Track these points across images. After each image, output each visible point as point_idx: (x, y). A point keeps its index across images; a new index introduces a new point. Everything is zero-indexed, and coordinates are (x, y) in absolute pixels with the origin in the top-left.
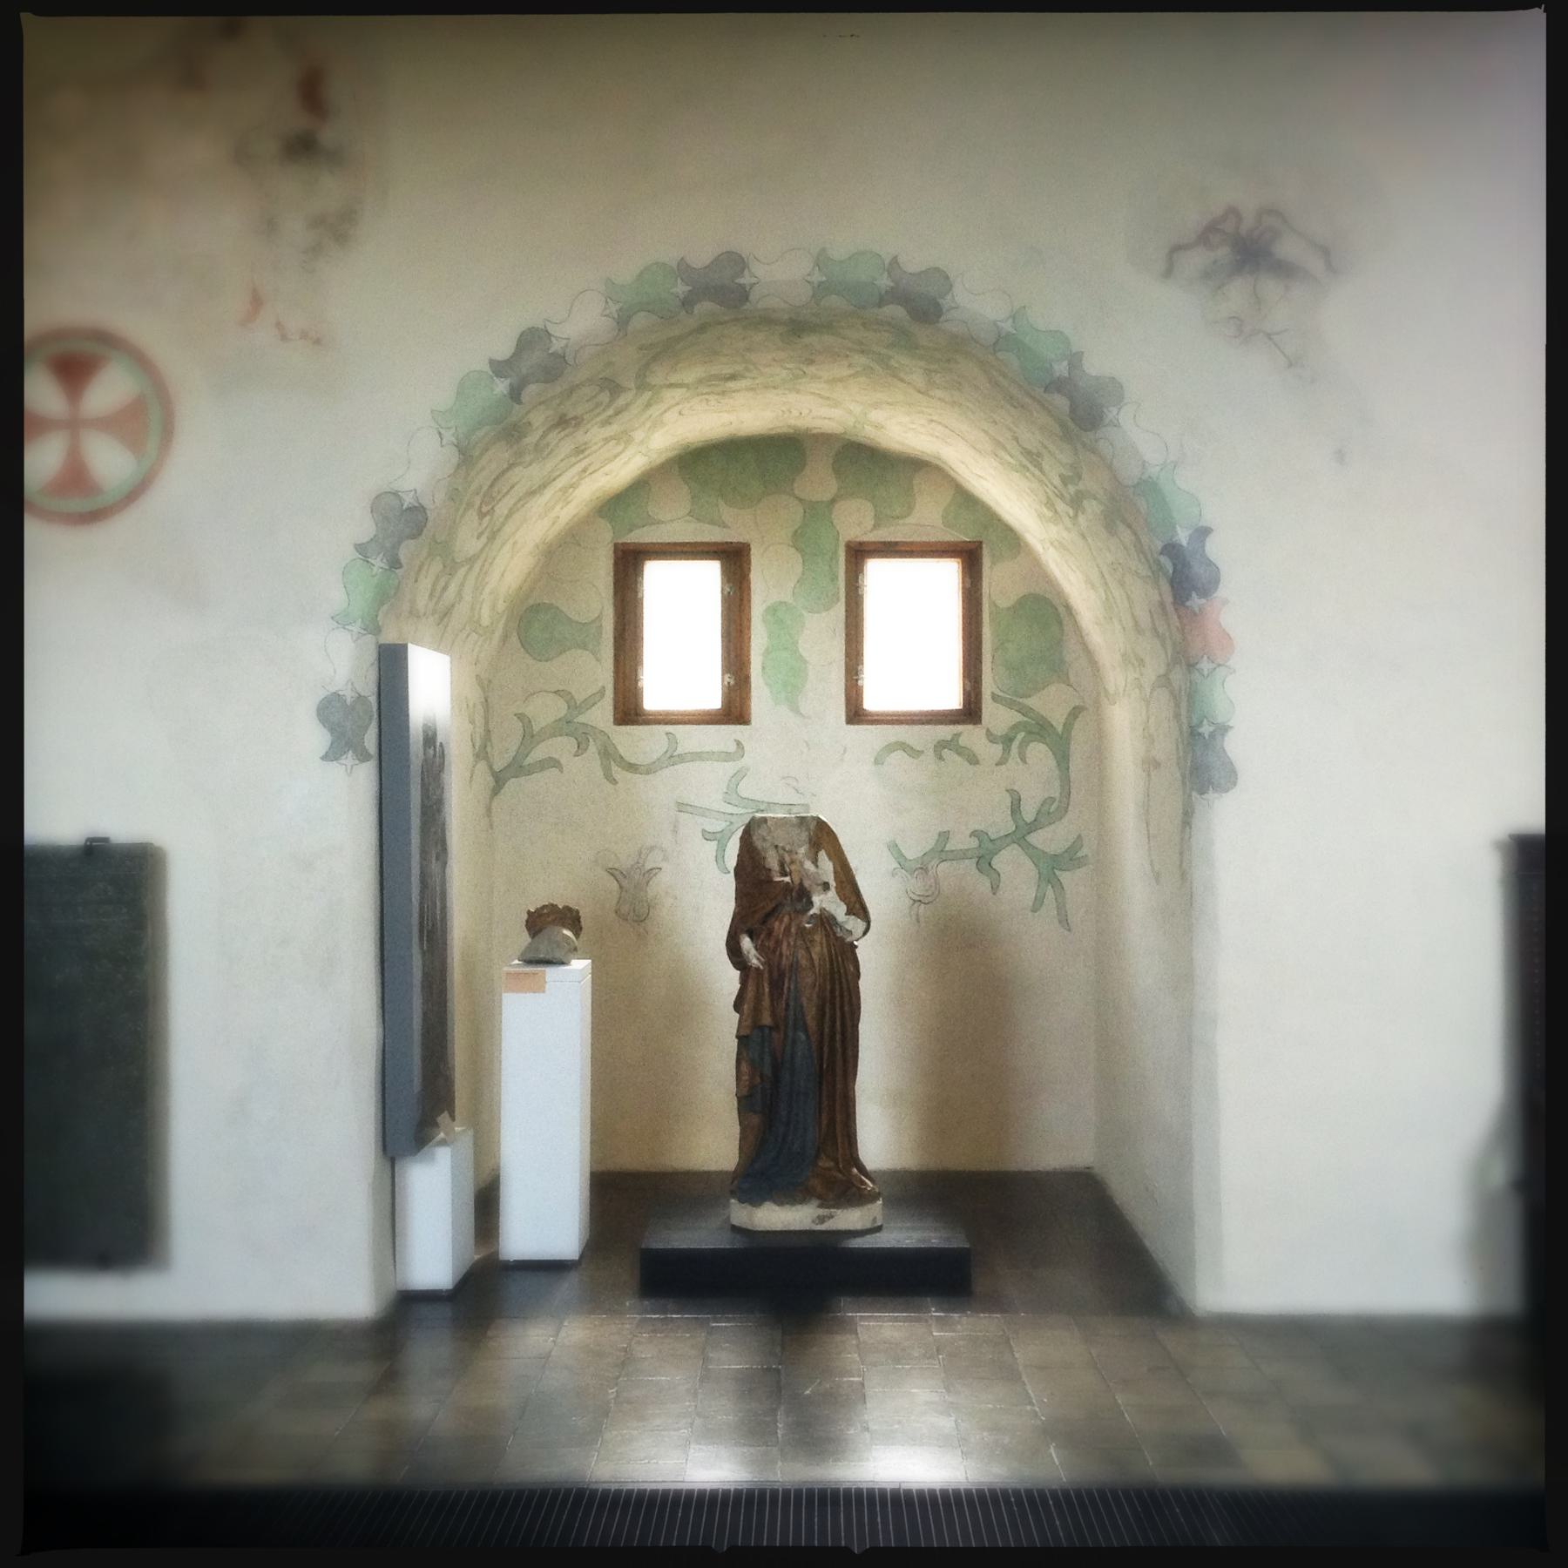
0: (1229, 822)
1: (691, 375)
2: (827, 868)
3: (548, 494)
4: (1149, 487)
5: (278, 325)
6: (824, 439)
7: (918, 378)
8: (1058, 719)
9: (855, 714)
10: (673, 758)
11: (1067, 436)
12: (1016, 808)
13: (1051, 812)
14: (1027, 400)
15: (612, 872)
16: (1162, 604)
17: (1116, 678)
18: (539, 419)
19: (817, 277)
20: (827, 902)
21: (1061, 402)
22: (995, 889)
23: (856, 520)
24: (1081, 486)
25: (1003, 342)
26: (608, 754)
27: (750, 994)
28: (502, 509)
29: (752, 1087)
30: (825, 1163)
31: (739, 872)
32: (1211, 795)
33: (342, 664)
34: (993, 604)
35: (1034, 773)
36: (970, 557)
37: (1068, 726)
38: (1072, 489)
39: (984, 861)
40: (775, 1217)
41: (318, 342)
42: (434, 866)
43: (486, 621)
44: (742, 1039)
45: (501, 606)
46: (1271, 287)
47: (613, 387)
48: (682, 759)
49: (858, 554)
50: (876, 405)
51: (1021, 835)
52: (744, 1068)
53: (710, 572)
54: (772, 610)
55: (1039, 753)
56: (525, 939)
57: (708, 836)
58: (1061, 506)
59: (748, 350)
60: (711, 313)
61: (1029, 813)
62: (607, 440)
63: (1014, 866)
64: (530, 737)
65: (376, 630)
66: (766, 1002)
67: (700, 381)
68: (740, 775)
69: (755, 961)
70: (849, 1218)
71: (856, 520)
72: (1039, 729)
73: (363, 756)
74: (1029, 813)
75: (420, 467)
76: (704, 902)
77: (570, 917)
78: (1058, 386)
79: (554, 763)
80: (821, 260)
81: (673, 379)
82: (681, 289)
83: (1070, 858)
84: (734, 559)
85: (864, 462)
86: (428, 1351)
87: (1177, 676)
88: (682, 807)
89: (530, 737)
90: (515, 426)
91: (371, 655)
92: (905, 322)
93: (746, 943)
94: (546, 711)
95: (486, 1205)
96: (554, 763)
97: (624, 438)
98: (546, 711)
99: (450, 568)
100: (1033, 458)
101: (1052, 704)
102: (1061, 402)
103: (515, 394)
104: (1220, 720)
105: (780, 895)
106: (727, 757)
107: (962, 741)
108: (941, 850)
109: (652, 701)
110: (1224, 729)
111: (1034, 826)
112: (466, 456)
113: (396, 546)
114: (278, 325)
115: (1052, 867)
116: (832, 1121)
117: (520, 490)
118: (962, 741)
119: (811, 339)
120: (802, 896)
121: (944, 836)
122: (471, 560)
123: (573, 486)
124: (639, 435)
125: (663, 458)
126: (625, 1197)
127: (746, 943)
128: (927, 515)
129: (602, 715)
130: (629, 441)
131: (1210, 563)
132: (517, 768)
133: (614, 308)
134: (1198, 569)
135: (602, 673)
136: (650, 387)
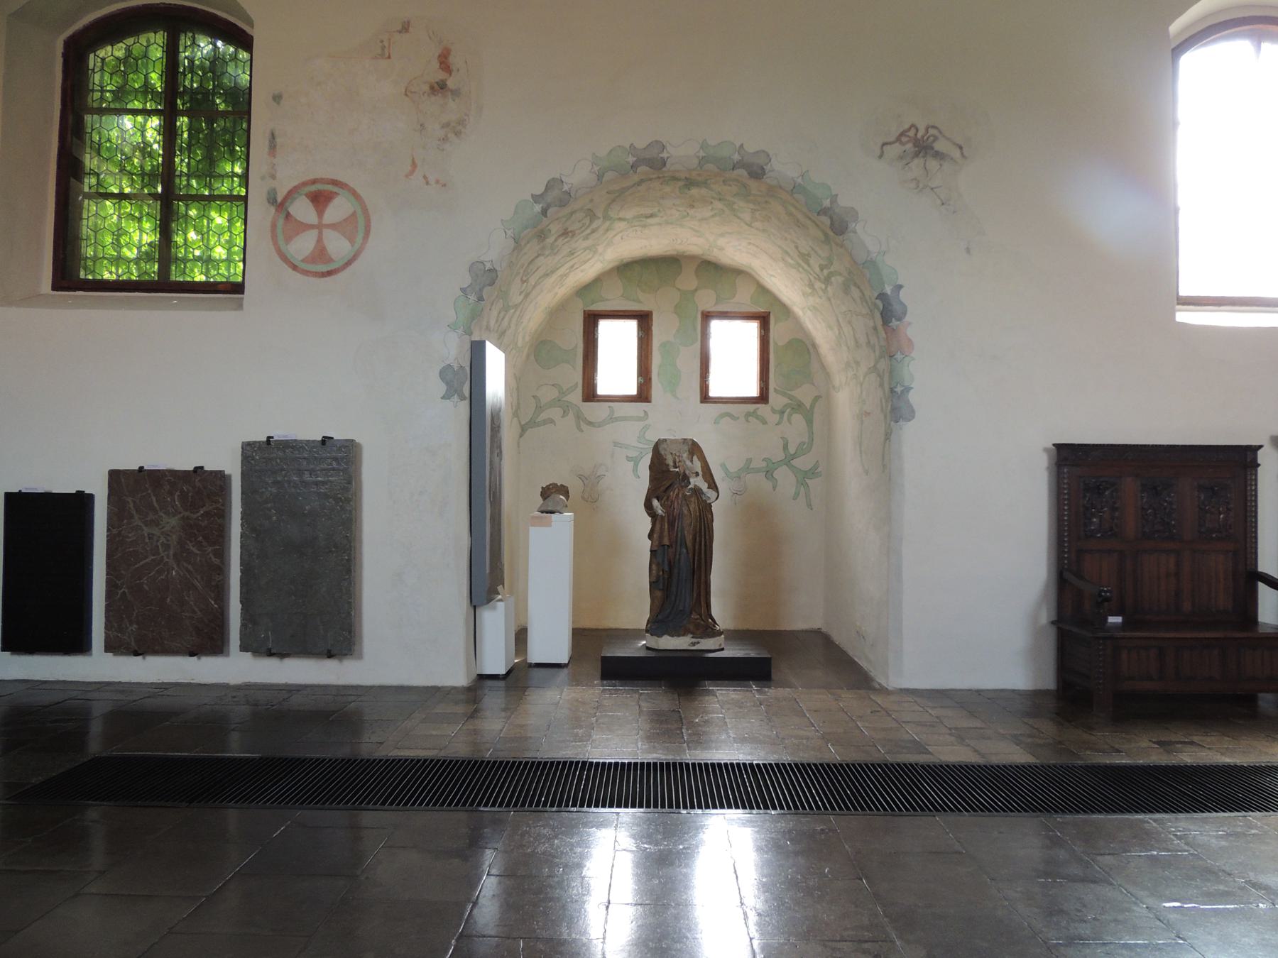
0: (909, 432)
1: (629, 214)
2: (697, 465)
3: (554, 277)
4: (872, 264)
5: (425, 177)
6: (692, 258)
7: (747, 216)
8: (807, 403)
9: (705, 398)
10: (612, 419)
11: (827, 240)
12: (786, 447)
13: (804, 449)
14: (809, 222)
15: (580, 477)
16: (875, 328)
17: (839, 378)
18: (555, 228)
19: (702, 154)
20: (698, 482)
21: (826, 220)
22: (774, 488)
23: (706, 300)
24: (832, 269)
25: (796, 188)
26: (579, 417)
27: (658, 526)
28: (532, 281)
29: (658, 577)
30: (694, 616)
31: (652, 467)
32: (901, 423)
33: (453, 351)
34: (776, 344)
35: (795, 428)
36: (764, 320)
37: (813, 406)
38: (826, 272)
39: (769, 474)
40: (669, 643)
41: (444, 185)
42: (496, 459)
43: (520, 344)
44: (653, 552)
45: (527, 339)
46: (933, 164)
47: (591, 215)
48: (617, 419)
49: (707, 317)
50: (722, 235)
51: (788, 460)
52: (654, 567)
53: (631, 326)
54: (663, 345)
55: (797, 418)
56: (541, 501)
57: (629, 459)
58: (818, 285)
59: (663, 198)
60: (648, 175)
61: (792, 450)
62: (585, 249)
63: (785, 477)
64: (539, 408)
65: (469, 332)
66: (666, 533)
67: (635, 217)
68: (646, 428)
69: (660, 512)
70: (707, 644)
71: (706, 300)
72: (798, 407)
73: (462, 398)
74: (792, 450)
75: (494, 250)
76: (629, 490)
77: (564, 490)
78: (824, 211)
79: (552, 421)
80: (704, 146)
81: (621, 215)
82: (631, 159)
83: (813, 473)
84: (644, 320)
85: (711, 269)
86: (493, 700)
87: (883, 365)
88: (616, 444)
89: (539, 408)
90: (542, 231)
91: (468, 346)
92: (743, 180)
93: (655, 503)
94: (548, 394)
95: (521, 637)
96: (552, 421)
97: (592, 249)
98: (548, 394)
99: (506, 309)
100: (805, 257)
101: (804, 394)
102: (826, 220)
103: (544, 212)
104: (906, 384)
105: (670, 480)
106: (639, 419)
107: (759, 413)
108: (747, 468)
109: (601, 390)
110: (908, 389)
111: (794, 457)
112: (518, 244)
113: (481, 290)
114: (425, 177)
115: (804, 477)
116: (699, 595)
117: (540, 272)
118: (759, 413)
119: (694, 191)
120: (685, 478)
121: (749, 461)
122: (516, 306)
123: (566, 275)
124: (600, 249)
125: (611, 266)
126: (584, 639)
127: (655, 503)
128: (744, 298)
129: (576, 396)
130: (595, 252)
131: (902, 303)
132: (532, 423)
133: (596, 169)
134: (896, 307)
135: (577, 377)
136: (610, 219)
